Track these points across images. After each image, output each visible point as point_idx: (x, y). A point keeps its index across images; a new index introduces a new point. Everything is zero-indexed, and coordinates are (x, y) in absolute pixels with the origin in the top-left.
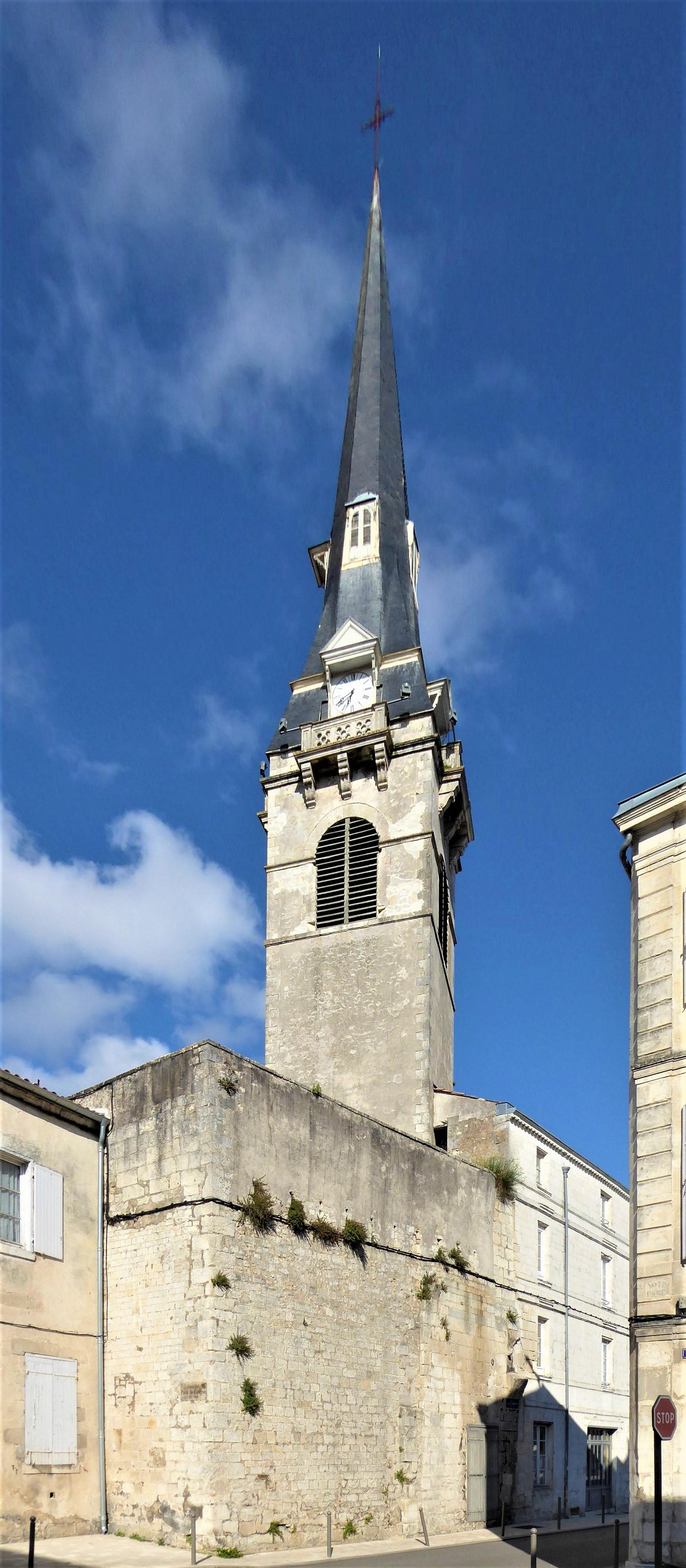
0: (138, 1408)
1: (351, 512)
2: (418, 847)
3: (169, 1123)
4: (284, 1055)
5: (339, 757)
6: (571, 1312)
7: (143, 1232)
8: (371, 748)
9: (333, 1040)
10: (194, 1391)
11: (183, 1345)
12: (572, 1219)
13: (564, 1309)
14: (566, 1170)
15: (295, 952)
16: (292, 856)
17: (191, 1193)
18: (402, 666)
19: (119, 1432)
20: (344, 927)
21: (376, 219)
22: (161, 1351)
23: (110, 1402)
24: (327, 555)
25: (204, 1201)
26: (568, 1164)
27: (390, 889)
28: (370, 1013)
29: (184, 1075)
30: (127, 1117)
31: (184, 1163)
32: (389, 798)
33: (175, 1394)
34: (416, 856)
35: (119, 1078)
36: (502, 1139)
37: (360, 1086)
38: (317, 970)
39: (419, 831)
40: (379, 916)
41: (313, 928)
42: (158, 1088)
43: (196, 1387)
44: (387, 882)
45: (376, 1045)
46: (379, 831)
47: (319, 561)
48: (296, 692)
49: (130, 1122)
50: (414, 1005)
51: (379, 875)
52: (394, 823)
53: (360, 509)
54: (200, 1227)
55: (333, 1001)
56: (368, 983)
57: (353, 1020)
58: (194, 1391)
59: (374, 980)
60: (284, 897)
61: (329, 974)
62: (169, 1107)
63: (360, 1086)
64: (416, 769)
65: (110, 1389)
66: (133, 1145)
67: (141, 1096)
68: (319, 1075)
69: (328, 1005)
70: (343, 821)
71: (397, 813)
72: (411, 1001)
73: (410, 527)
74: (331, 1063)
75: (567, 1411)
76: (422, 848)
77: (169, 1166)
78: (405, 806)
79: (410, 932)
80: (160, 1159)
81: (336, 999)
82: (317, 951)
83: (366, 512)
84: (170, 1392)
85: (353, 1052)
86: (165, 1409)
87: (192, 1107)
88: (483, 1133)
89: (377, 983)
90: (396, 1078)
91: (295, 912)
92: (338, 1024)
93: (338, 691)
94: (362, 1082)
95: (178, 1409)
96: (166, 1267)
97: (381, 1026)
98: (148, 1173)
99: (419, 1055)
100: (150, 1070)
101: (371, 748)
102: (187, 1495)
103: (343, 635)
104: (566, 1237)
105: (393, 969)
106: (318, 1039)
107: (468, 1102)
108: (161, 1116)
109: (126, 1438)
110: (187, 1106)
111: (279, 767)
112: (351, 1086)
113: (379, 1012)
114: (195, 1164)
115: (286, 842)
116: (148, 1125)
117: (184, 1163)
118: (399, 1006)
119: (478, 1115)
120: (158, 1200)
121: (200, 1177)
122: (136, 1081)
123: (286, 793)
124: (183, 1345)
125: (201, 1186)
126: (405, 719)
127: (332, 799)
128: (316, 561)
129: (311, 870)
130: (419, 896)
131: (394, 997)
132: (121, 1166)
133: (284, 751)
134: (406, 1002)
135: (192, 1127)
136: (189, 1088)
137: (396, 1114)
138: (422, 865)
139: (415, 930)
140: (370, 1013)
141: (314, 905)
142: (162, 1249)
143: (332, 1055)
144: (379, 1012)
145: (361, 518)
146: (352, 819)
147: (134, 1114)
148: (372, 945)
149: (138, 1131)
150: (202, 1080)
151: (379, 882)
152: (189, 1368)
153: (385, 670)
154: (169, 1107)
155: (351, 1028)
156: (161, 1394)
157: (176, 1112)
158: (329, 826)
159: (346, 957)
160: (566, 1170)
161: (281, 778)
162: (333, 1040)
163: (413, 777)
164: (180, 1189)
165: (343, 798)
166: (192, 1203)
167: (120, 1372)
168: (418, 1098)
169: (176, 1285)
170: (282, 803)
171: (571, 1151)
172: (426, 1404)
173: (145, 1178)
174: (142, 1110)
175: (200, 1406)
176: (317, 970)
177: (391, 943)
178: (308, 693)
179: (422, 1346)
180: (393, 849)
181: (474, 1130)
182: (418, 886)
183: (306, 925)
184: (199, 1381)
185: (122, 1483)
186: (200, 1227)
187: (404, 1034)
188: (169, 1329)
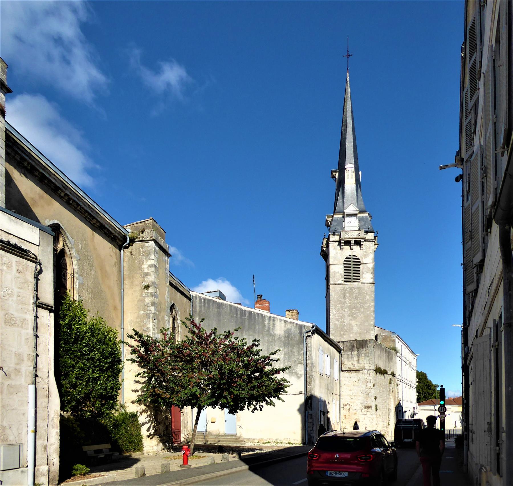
0: (351, 410)
1: (347, 169)
2: (371, 266)
3: (361, 353)
4: (335, 314)
5: (352, 241)
6: (403, 382)
7: (353, 374)
8: (360, 241)
9: (349, 312)
10: (369, 407)
11: (365, 398)
12: (403, 359)
13: (402, 381)
14: (402, 346)
15: (338, 288)
16: (336, 262)
17: (367, 368)
18: (364, 216)
19: (345, 416)
20: (352, 283)
21: (349, 84)
22: (358, 399)
23: (342, 409)
24: (337, 174)
25: (371, 370)
26: (402, 344)
27: (364, 275)
28: (359, 306)
29: (366, 344)
30: (348, 350)
31: (365, 362)
32: (363, 252)
33: (362, 408)
34: (371, 268)
35: (346, 341)
36: (394, 341)
37: (356, 325)
38: (344, 293)
39: (371, 262)
40: (361, 281)
41: (343, 282)
42: (358, 346)
43: (369, 406)
44: (363, 273)
45: (360, 315)
46: (361, 260)
47: (334, 175)
48: (335, 216)
49: (349, 351)
50: (371, 306)
51: (361, 271)
52: (365, 258)
53: (350, 169)
54: (370, 375)
55: (349, 302)
56: (358, 298)
57: (354, 307)
58: (369, 407)
59: (360, 298)
60: (335, 273)
61: (348, 295)
62: (361, 350)
63: (356, 325)
64: (370, 246)
65: (342, 406)
66: (350, 356)
67: (353, 346)
68: (345, 321)
69: (348, 303)
70: (351, 255)
71: (365, 256)
72: (370, 305)
73: (360, 173)
74: (349, 318)
75: (402, 407)
76: (372, 266)
77: (361, 362)
78: (367, 255)
79: (369, 287)
80: (358, 360)
81: (350, 301)
82: (344, 288)
83: (351, 171)
84: (361, 407)
85: (354, 316)
86: (360, 411)
87: (367, 351)
88: (388, 339)
89: (361, 299)
90: (366, 324)
91: (338, 277)
92: (351, 308)
93: (347, 219)
94: (357, 324)
95: (363, 411)
96: (360, 382)
97: (362, 310)
98: (355, 362)
99: (372, 318)
100: (355, 341)
101: (360, 241)
102: (366, 428)
103: (491, 392)
104: (402, 362)
105: (365, 296)
106: (345, 311)
107: (384, 331)
108: (359, 351)
109: (347, 417)
110: (366, 350)
111: (333, 238)
112: (354, 324)
113: (361, 306)
114: (369, 362)
115: (335, 258)
116: (355, 353)
117: (365, 362)
118: (367, 305)
119: (387, 334)
120: (357, 368)
121: (370, 365)
122: (351, 343)
123: (335, 245)
124: (365, 398)
125: (370, 367)
126: (367, 232)
127: (348, 249)
128: (333, 175)
129: (342, 267)
130: (372, 278)
131: (365, 303)
132: (346, 360)
133: (334, 234)
134: (369, 305)
135: (367, 355)
136: (366, 347)
137: (366, 333)
138: (372, 271)
139: (371, 287)
140: (359, 306)
141: (343, 276)
142: (359, 378)
143: (349, 316)
144: (361, 306)
145: (350, 171)
146: (353, 255)
147: (350, 349)
148: (359, 289)
149: (352, 353)
150: (370, 346)
151: (361, 273)
152: (367, 402)
153: (359, 216)
154: (361, 350)
155: (354, 309)
156: (359, 408)
157: (363, 351)
158: (347, 256)
159: (352, 291)
160: (402, 346)
161: (334, 241)
162: (349, 312)
163: (369, 248)
164: (364, 367)
165: (351, 250)
166: (368, 370)
167: (346, 403)
168: (372, 329)
169: (363, 386)
170: (334, 248)
171: (402, 340)
172: (391, 408)
173: (354, 363)
174: (353, 349)
175: (370, 410)
176: (344, 293)
177: (364, 289)
178: (338, 218)
179: (390, 395)
180: (364, 265)
181: (385, 338)
182: (371, 276)
183: (341, 281)
184: (370, 405)
185: (346, 426)
186: (370, 375)
187: (368, 313)
188: (361, 394)
